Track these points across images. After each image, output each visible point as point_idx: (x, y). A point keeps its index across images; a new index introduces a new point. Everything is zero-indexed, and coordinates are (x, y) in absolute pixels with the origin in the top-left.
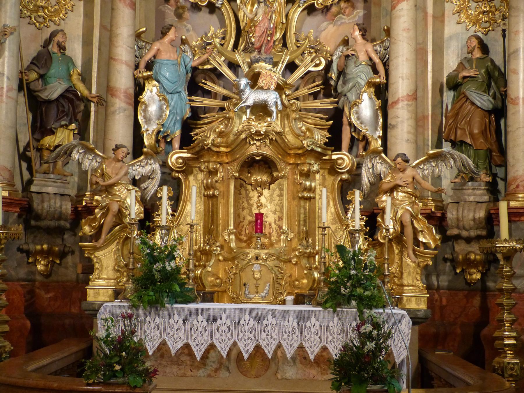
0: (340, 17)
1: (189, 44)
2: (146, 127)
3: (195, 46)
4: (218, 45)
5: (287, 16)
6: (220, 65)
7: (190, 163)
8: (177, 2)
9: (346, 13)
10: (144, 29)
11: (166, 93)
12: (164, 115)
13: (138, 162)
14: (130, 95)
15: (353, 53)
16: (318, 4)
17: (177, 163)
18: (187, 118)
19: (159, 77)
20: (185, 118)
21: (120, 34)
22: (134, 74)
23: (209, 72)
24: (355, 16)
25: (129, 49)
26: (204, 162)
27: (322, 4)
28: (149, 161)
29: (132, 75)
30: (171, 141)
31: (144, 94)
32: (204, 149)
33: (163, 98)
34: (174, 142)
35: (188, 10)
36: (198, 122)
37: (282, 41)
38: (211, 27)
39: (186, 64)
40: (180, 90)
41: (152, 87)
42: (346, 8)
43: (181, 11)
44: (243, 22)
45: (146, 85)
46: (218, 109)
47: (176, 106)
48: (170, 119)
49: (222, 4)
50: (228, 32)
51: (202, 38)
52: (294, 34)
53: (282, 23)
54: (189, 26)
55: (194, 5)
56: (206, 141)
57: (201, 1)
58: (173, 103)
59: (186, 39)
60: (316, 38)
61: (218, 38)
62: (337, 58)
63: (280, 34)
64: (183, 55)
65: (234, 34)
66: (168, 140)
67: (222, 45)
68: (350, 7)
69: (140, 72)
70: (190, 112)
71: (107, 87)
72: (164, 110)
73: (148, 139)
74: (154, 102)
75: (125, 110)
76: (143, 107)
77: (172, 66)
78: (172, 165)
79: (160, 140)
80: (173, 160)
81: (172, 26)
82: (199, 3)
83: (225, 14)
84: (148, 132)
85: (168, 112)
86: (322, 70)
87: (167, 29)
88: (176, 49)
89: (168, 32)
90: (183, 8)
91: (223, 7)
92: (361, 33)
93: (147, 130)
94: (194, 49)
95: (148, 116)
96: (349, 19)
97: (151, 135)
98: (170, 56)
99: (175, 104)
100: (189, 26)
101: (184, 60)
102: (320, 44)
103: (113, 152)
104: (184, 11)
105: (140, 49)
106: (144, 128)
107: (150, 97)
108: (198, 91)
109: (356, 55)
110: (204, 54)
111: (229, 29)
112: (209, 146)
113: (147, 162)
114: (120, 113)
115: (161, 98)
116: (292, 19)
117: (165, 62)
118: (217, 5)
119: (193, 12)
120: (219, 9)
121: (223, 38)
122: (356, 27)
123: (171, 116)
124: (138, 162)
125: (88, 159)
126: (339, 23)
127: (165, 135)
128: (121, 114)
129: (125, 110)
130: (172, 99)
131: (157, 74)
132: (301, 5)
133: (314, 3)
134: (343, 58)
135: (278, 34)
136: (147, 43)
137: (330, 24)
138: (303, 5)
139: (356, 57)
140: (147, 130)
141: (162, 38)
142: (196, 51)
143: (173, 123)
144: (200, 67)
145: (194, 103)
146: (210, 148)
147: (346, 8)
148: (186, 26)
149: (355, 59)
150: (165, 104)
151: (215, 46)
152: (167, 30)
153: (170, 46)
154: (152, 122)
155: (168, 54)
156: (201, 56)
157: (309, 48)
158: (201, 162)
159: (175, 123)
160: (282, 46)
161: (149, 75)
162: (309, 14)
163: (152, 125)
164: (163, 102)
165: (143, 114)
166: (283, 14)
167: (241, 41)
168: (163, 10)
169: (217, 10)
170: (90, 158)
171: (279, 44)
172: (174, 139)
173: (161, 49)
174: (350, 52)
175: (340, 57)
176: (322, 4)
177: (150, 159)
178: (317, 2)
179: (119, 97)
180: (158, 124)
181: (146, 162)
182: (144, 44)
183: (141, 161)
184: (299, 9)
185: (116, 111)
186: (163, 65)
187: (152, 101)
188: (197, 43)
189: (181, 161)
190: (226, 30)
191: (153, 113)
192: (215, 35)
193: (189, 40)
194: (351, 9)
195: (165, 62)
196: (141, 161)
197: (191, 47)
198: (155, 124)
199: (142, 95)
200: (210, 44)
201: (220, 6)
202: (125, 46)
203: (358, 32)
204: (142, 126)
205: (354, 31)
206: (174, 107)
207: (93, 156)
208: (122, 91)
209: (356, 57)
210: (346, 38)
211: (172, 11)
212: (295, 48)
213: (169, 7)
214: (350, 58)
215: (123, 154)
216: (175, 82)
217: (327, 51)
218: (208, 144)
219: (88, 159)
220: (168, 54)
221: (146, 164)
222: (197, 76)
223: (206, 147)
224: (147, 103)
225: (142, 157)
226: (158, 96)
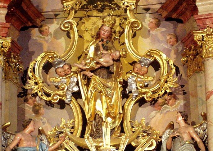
0: (165, 107)
1: (45, 134)
3: (50, 135)
4: (69, 134)
5: (123, 107)
6: (72, 148)
9: (170, 104)
10: (9, 123)
15: (178, 134)
16: (147, 98)
24: (177, 106)
27: (150, 97)
37: (120, 128)
38: (63, 119)
42: (170, 99)
43: (37, 108)
44: (88, 114)
50: (76, 123)
51: (55, 129)
52: (130, 122)
53: (120, 114)
54: (45, 120)
59: (42, 130)
60: (147, 124)
61: (69, 128)
62: (166, 139)
63: (119, 122)
65: (81, 124)
67: (72, 133)
68: (173, 99)
81: (31, 120)
82: (52, 101)
83: (74, 108)
86: (153, 150)
89: (28, 125)
90: (39, 105)
92: (183, 119)
96: (173, 108)
100: (45, 120)
102: (151, 128)
104: (41, 108)
109: (181, 136)
110: (57, 141)
111: (77, 120)
116: (127, 110)
118: (67, 102)
120: (68, 104)
121: (73, 128)
122: (179, 114)
126: (165, 112)
132: (134, 99)
133: (144, 97)
134: (170, 139)
135: (117, 122)
136: (11, 134)
137: (158, 112)
138: (135, 99)
139: (181, 138)
142: (50, 139)
147: (170, 99)
148: (42, 120)
149: (181, 139)
151: (66, 135)
152: (27, 124)
153: (30, 136)
160: (121, 132)
162: (140, 106)
166: (120, 106)
167: (87, 129)
171: (118, 130)
173: (23, 139)
174: (176, 134)
175: (168, 138)
176: (150, 97)
178: (146, 96)
182: (9, 135)
184: (133, 102)
188: (52, 133)
190: (75, 121)
192: (66, 126)
193: (45, 131)
194: (174, 100)
197: (46, 136)
200: (62, 133)
201: (69, 102)
203: (181, 118)
205: (178, 117)
209: (181, 138)
210: (172, 123)
212: (131, 133)
213: (28, 105)
214: (176, 139)
217: (157, 134)
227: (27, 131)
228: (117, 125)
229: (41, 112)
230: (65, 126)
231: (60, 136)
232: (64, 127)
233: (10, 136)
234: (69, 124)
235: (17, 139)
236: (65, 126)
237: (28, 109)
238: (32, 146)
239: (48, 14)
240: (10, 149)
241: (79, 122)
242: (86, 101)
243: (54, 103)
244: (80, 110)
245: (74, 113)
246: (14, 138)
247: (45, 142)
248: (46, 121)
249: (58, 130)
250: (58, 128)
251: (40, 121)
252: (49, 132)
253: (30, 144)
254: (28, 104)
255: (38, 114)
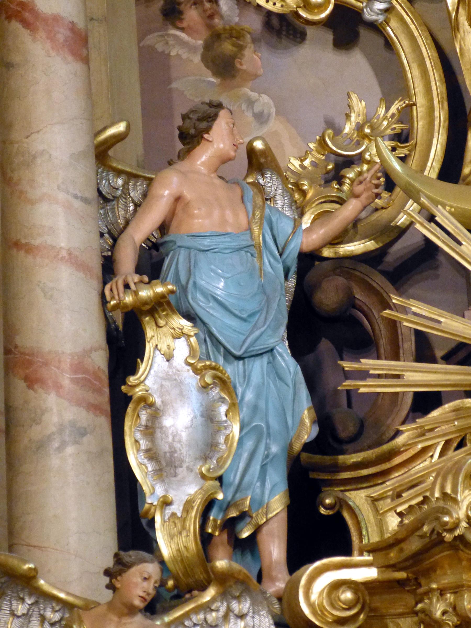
2: (160, 491)
7: (377, 602)
8: (211, 17)
10: (121, 127)
11: (221, 360)
12: (222, 439)
13: (196, 610)
14: (95, 375)
17: (333, 606)
18: (307, 447)
19: (194, 299)
20: (297, 447)
21: (43, 152)
22: (103, 296)
23: (364, 268)
25: (77, 204)
26: (442, 592)
28: (235, 605)
29: (95, 299)
30: (253, 537)
31: (142, 368)
32: (440, 541)
33: (215, 377)
34: (263, 537)
35: (254, 41)
36: (341, 458)
38: (354, 97)
39: (281, 242)
40: (271, 342)
41: (169, 340)
45: (149, 332)
46: (409, 401)
47: (262, 404)
48: (245, 456)
49: (386, 11)
51: (322, 143)
55: (275, 22)
56: (448, 513)
57: (307, 6)
58: (249, 396)
59: (267, 152)
64: (267, 211)
66: (245, 535)
69: (127, 286)
70: (313, 422)
71: (7, 351)
72: (220, 422)
73: (172, 537)
74: (182, 395)
75: (82, 432)
76: (144, 416)
77: (235, 258)
78: (314, 613)
79: (211, 536)
80: (314, 597)
81: (219, 106)
84: (169, 511)
85: (236, 429)
87: (200, 120)
88: (238, 191)
89: (208, 130)
91: (394, 23)
93: (166, 503)
94: (297, 186)
95: (166, 448)
97: (184, 520)
98: (223, 221)
99: (258, 396)
101: (271, 229)
103: (106, 580)
104: (241, 48)
105: (106, 200)
106: (153, 493)
107: (167, 377)
108: (319, 341)
110: (341, 202)
112: (458, 532)
113: (229, 610)
114: (63, 444)
115: (208, 380)
117: (207, 242)
118: (369, 15)
119: (273, 47)
123: (249, 444)
124: (196, 610)
125: (13, 614)
127: (233, 514)
128: (70, 450)
129: (82, 432)
130: (247, 377)
131: (184, 289)
136: (131, 176)
140: (166, 503)
141: (183, 155)
142: (304, 193)
143: (256, 468)
144: (327, 253)
145: (370, 382)
146: (461, 538)
148: (251, 103)
150: (222, 400)
152: (203, 125)
153: (218, 181)
154: (182, 471)
155: (216, 213)
156: (328, 207)
157: (392, 119)
158: (431, 590)
159: (263, 468)
161: (163, 296)
163: (182, 482)
164: (216, 392)
165: (144, 444)
168: (160, 47)
169: (363, 32)
170: (21, 609)
172: (265, 530)
173: (188, 195)
177: (238, 598)
179: (58, 387)
180: (203, 477)
181: (223, 609)
182: (120, 182)
183: (207, 608)
185: (49, 438)
186: (201, 256)
187: (175, 392)
188: (307, 163)
189: (348, 595)
190: (410, 106)
191: (184, 436)
195: (207, 242)
196: (207, 608)
197: (285, 180)
198: (191, 477)
199: (133, 370)
201: (381, 18)
202: (61, 196)
204: (145, 488)
206: (255, 409)
207: (29, 601)
208: (67, 363)
211: (193, 49)
213: (183, 35)
215: (145, 584)
216: (252, 315)
218: (456, 525)
219: (13, 614)
220: (216, 213)
221: (226, 617)
222: (316, 286)
223: (448, 537)
224: (157, 399)
225: (210, 593)
226: (196, 371)
227: (204, 158)
228: (120, 209)
229: (244, 67)
230: (367, 131)
231: (351, 174)
232: (366, 136)
233: (123, 186)
234: (385, 118)
235: (163, 196)
236: (367, 131)
237: (185, 56)
238: (229, 230)
239: (406, 6)
240: (135, 243)
241: (431, 109)
242: (461, 11)
243: (308, 22)
244: (436, 55)
245: (407, 68)
246: (145, 195)
247: (279, 207)
248: (273, 110)
249: (334, 148)
250: (332, 140)
251: (244, 107)
252: (292, 160)
253: (349, 179)
254: (182, 29)
255: (234, 77)
